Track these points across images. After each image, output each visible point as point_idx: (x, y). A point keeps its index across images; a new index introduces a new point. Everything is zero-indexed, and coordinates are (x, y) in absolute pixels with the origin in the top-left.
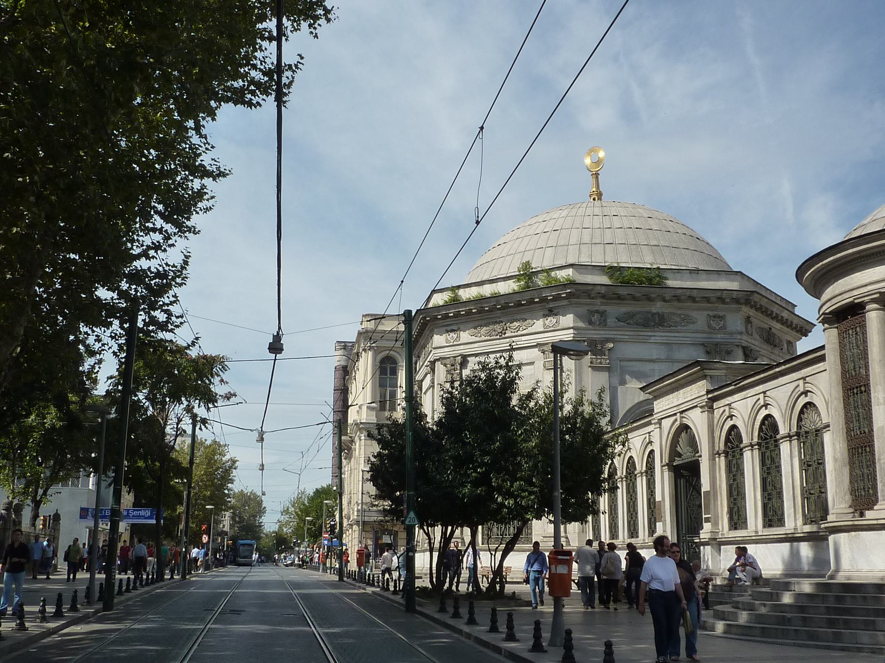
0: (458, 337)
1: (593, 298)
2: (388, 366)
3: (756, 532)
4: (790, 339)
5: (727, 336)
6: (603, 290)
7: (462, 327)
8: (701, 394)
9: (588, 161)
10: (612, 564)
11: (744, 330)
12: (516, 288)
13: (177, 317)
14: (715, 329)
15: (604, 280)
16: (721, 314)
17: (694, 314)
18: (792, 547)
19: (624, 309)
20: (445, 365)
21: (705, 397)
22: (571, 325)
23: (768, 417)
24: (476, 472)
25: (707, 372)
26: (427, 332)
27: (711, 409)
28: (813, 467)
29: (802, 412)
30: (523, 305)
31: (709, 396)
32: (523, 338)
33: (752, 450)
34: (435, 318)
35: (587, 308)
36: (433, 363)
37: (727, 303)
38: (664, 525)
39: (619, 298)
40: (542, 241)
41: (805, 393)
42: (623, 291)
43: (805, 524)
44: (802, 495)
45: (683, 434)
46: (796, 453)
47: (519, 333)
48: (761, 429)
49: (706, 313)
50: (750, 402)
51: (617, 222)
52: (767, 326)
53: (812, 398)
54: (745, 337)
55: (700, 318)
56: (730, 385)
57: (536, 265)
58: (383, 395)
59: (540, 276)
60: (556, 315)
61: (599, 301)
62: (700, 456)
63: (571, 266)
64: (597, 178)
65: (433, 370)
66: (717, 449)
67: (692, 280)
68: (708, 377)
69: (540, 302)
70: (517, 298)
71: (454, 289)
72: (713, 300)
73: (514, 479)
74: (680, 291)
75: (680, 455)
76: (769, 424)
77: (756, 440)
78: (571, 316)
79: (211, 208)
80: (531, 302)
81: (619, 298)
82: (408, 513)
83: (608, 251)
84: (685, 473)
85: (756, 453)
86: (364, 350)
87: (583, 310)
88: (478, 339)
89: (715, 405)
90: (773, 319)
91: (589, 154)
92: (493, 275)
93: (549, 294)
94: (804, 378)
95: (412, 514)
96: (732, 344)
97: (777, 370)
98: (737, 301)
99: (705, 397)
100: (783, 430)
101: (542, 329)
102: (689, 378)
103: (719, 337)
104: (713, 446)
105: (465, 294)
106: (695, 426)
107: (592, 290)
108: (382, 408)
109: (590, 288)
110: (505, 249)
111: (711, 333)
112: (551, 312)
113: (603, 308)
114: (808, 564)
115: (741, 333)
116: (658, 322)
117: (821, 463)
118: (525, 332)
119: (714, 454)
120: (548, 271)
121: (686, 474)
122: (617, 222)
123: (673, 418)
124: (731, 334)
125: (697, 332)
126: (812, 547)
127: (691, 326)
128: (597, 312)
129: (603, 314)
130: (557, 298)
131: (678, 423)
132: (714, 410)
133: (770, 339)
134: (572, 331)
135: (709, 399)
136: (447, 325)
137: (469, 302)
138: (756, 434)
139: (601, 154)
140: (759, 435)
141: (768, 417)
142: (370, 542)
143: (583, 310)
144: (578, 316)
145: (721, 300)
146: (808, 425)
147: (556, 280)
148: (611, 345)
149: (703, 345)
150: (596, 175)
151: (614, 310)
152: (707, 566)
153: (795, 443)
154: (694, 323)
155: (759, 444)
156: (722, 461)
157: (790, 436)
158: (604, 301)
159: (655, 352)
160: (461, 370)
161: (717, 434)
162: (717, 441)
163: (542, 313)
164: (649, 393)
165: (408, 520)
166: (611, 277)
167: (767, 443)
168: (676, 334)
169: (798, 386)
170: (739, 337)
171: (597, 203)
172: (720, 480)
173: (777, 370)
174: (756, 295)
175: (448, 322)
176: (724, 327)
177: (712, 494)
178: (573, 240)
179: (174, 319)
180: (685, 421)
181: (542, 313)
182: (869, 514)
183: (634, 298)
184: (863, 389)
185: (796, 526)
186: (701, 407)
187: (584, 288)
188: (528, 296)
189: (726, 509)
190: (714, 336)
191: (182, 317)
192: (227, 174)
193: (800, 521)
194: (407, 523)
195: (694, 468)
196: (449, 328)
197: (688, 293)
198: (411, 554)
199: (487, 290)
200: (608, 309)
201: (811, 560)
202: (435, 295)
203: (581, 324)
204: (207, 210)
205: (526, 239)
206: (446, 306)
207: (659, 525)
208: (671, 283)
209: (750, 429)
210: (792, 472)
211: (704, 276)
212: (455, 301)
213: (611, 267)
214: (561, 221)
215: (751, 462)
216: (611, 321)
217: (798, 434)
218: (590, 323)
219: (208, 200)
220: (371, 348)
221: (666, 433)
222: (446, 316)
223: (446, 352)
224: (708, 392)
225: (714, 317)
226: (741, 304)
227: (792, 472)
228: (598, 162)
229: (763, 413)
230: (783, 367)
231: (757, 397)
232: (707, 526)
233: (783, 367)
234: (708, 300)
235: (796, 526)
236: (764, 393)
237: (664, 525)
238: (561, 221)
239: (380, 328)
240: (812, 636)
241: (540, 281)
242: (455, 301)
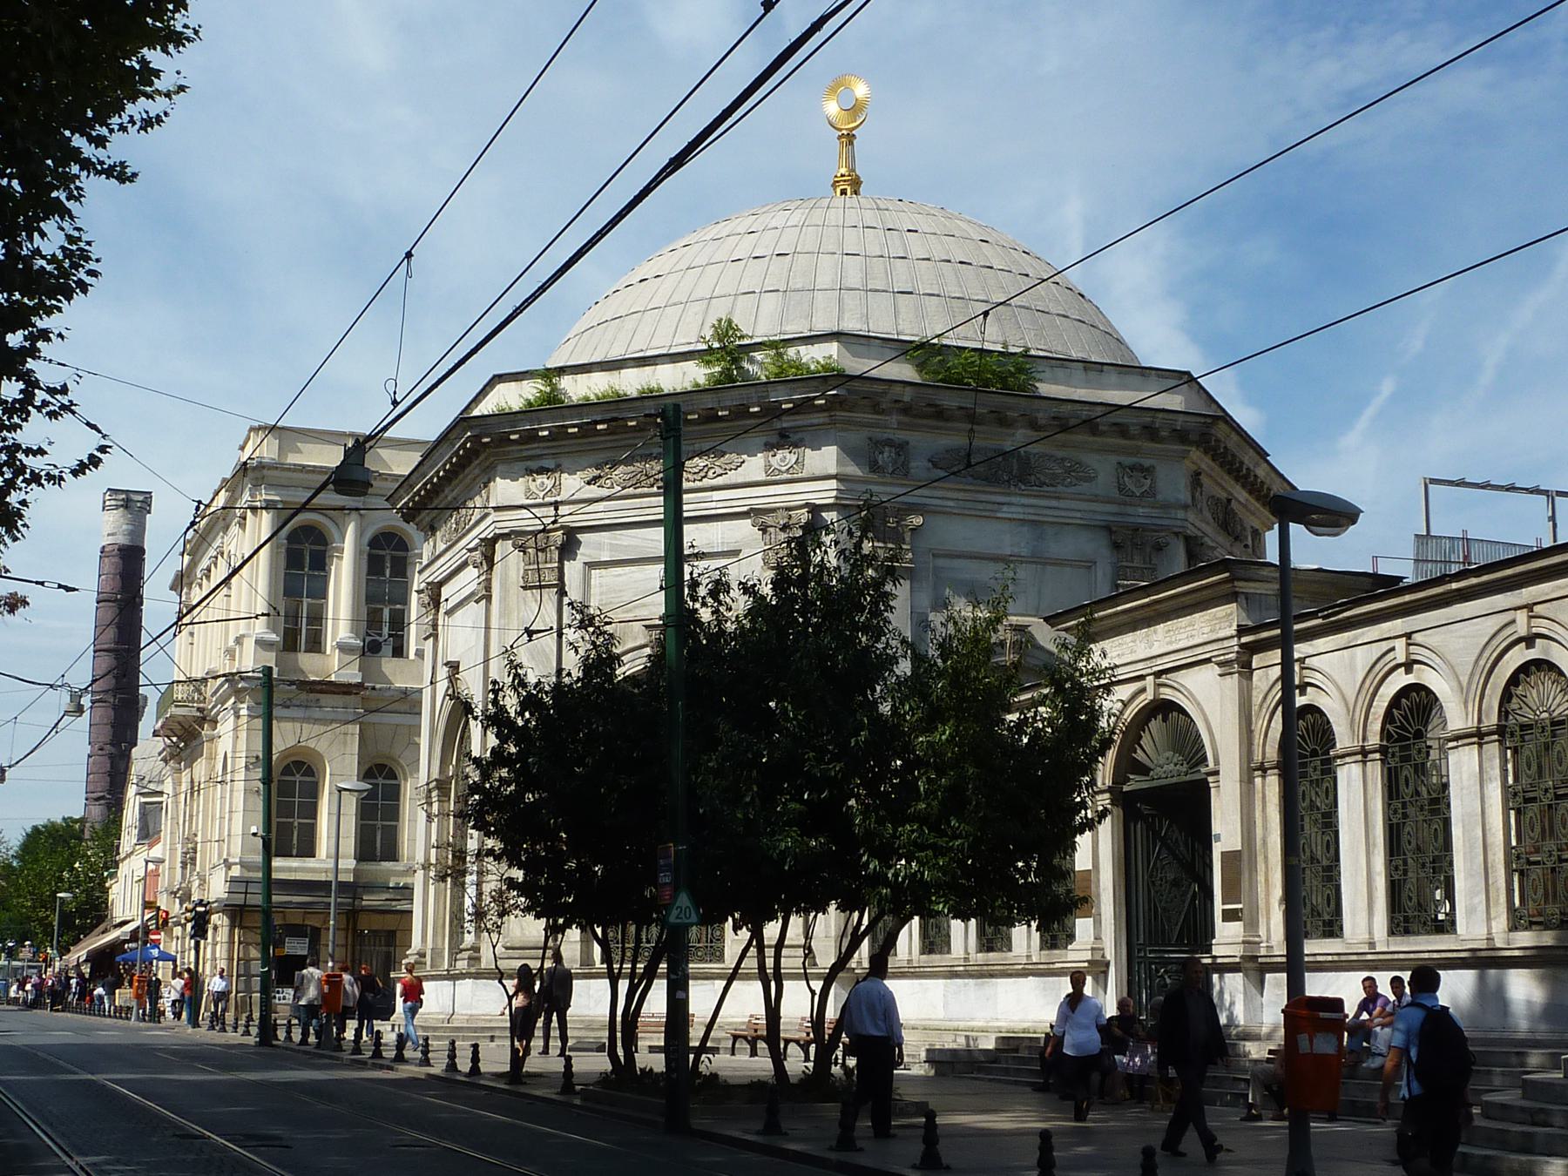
0: (557, 486)
1: (883, 412)
2: (307, 548)
3: (1372, 944)
4: (1257, 525)
5: (1155, 512)
6: (907, 395)
7: (566, 462)
8: (1222, 634)
9: (832, 108)
10: (872, 1009)
11: (1189, 501)
12: (702, 381)
13: (52, 391)
14: (1133, 495)
15: (903, 371)
16: (1147, 463)
17: (1091, 460)
18: (1482, 980)
19: (952, 439)
20: (523, 549)
21: (1235, 641)
22: (833, 471)
24: (802, 801)
25: (1242, 586)
26: (473, 469)
27: (1246, 670)
29: (1514, 680)
30: (722, 419)
31: (1244, 640)
32: (717, 495)
33: (1364, 763)
34: (504, 440)
35: (865, 433)
36: (489, 544)
37: (1161, 440)
38: (1098, 924)
39: (940, 414)
40: (752, 277)
41: (1529, 641)
42: (950, 401)
43: (1513, 927)
44: (1508, 864)
45: (1155, 725)
47: (706, 482)
48: (1388, 717)
49: (1114, 459)
50: (1363, 658)
51: (916, 247)
52: (1224, 495)
53: (1546, 650)
54: (1191, 516)
56: (1313, 615)
57: (759, 324)
58: (293, 617)
59: (758, 356)
60: (796, 446)
61: (894, 419)
63: (836, 336)
64: (851, 143)
65: (490, 560)
66: (1258, 757)
67: (1088, 384)
68: (1242, 599)
70: (709, 402)
71: (550, 374)
72: (1134, 430)
73: (900, 820)
74: (1069, 406)
75: (1143, 770)
76: (1415, 707)
77: (1374, 740)
78: (834, 448)
79: (159, 120)
80: (741, 412)
81: (940, 414)
82: (674, 897)
83: (903, 310)
84: (1145, 809)
85: (1375, 769)
86: (254, 509)
87: (857, 437)
89: (1256, 661)
90: (1237, 479)
91: (833, 90)
92: (635, 346)
93: (784, 398)
94: (1529, 607)
95: (684, 900)
96: (1161, 528)
97: (1454, 586)
98: (1182, 436)
99: (1235, 641)
101: (762, 477)
102: (1187, 600)
103: (1141, 514)
105: (576, 388)
106: (1204, 715)
107: (885, 393)
108: (290, 643)
109: (880, 388)
110: (660, 292)
111: (1125, 504)
112: (784, 440)
113: (901, 436)
114: (1532, 1018)
115: (1185, 507)
116: (1011, 472)
118: (720, 481)
119: (1252, 770)
120: (778, 345)
122: (916, 247)
124: (1166, 506)
125: (1095, 499)
126: (1542, 979)
127: (1084, 487)
128: (889, 443)
129: (901, 448)
130: (803, 407)
131: (1149, 696)
132: (1252, 671)
133: (1227, 521)
134: (833, 484)
135: (1241, 646)
137: (585, 406)
138: (1376, 726)
139: (861, 90)
140: (1383, 729)
142: (254, 953)
143: (857, 437)
144: (848, 451)
145: (1151, 432)
147: (798, 366)
148: (918, 521)
150: (850, 138)
151: (927, 442)
152: (1231, 1017)
153: (1493, 749)
154: (1090, 479)
155: (1382, 750)
156: (1271, 786)
157: (1478, 736)
158: (906, 419)
159: (1007, 540)
160: (561, 562)
162: (1258, 740)
163: (764, 439)
164: (1066, 630)
165: (675, 912)
166: (921, 367)
167: (1402, 748)
168: (1054, 503)
169: (1513, 621)
170: (1181, 514)
171: (851, 200)
172: (1265, 828)
173: (1454, 586)
174: (1222, 425)
175: (534, 449)
176: (1152, 492)
177: (1245, 857)
178: (824, 280)
179: (40, 396)
180: (1166, 693)
181: (764, 439)
183: (971, 417)
185: (1489, 933)
186: (1220, 664)
187: (866, 387)
188: (732, 398)
189: (1277, 892)
190: (1130, 510)
191: (64, 390)
192: (189, 40)
193: (1500, 923)
194: (672, 919)
195: (1189, 804)
196: (534, 465)
197: (1085, 413)
198: (680, 995)
199: (631, 382)
201: (1538, 1009)
203: (853, 470)
204: (148, 123)
205: (712, 271)
206: (530, 411)
208: (1045, 389)
209: (1359, 716)
211: (1113, 377)
212: (552, 403)
213: (922, 346)
214: (790, 235)
215: (1358, 797)
216: (919, 466)
217: (1501, 731)
218: (874, 467)
219: (168, 95)
220: (269, 506)
222: (531, 437)
223: (523, 520)
224: (1242, 631)
225: (1132, 468)
226: (1191, 443)
228: (855, 109)
229: (1400, 680)
230: (1474, 581)
231: (1385, 646)
233: (1474, 581)
234: (1122, 431)
235: (1489, 933)
236: (1408, 636)
238: (790, 235)
239: (292, 459)
241: (759, 367)
242: (552, 403)
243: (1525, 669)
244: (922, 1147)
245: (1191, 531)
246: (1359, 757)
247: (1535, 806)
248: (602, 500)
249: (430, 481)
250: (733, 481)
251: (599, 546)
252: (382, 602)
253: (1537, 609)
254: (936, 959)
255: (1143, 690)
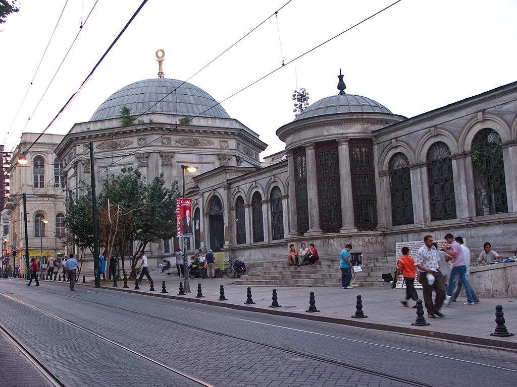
16: (226, 140)
23: (257, 192)
28: (277, 214)
29: (430, 149)
32: (127, 151)
36: (76, 163)
44: (272, 227)
46: (270, 209)
48: (253, 198)
49: (218, 139)
50: (248, 186)
55: (216, 142)
62: (224, 210)
69: (136, 132)
77: (251, 203)
88: (102, 150)
92: (109, 115)
100: (263, 199)
101: (137, 146)
103: (225, 152)
104: (230, 204)
106: (221, 197)
117: (281, 212)
119: (230, 209)
121: (216, 220)
123: (210, 192)
127: (212, 146)
128: (166, 138)
131: (212, 195)
136: (84, 143)
141: (257, 192)
146: (275, 197)
149: (217, 155)
156: (234, 213)
161: (232, 200)
176: (228, 146)
180: (216, 194)
182: (306, 234)
184: (304, 182)
195: (220, 218)
200: (172, 137)
202: (76, 127)
207: (202, 244)
210: (268, 217)
215: (248, 213)
216: (173, 143)
221: (206, 200)
227: (268, 217)
231: (252, 183)
232: (227, 243)
233: (502, 91)
236: (255, 181)
237: (205, 243)
240: (286, 283)
243: (434, 145)
244: (356, 310)
245: (237, 155)
246: (463, 156)
247: (438, 185)
248: (101, 152)
249: (71, 138)
250: (132, 147)
251: (101, 163)
252: (58, 174)
253: (398, 139)
254: (242, 245)
255: (211, 193)
